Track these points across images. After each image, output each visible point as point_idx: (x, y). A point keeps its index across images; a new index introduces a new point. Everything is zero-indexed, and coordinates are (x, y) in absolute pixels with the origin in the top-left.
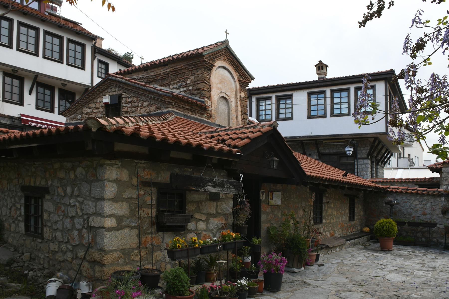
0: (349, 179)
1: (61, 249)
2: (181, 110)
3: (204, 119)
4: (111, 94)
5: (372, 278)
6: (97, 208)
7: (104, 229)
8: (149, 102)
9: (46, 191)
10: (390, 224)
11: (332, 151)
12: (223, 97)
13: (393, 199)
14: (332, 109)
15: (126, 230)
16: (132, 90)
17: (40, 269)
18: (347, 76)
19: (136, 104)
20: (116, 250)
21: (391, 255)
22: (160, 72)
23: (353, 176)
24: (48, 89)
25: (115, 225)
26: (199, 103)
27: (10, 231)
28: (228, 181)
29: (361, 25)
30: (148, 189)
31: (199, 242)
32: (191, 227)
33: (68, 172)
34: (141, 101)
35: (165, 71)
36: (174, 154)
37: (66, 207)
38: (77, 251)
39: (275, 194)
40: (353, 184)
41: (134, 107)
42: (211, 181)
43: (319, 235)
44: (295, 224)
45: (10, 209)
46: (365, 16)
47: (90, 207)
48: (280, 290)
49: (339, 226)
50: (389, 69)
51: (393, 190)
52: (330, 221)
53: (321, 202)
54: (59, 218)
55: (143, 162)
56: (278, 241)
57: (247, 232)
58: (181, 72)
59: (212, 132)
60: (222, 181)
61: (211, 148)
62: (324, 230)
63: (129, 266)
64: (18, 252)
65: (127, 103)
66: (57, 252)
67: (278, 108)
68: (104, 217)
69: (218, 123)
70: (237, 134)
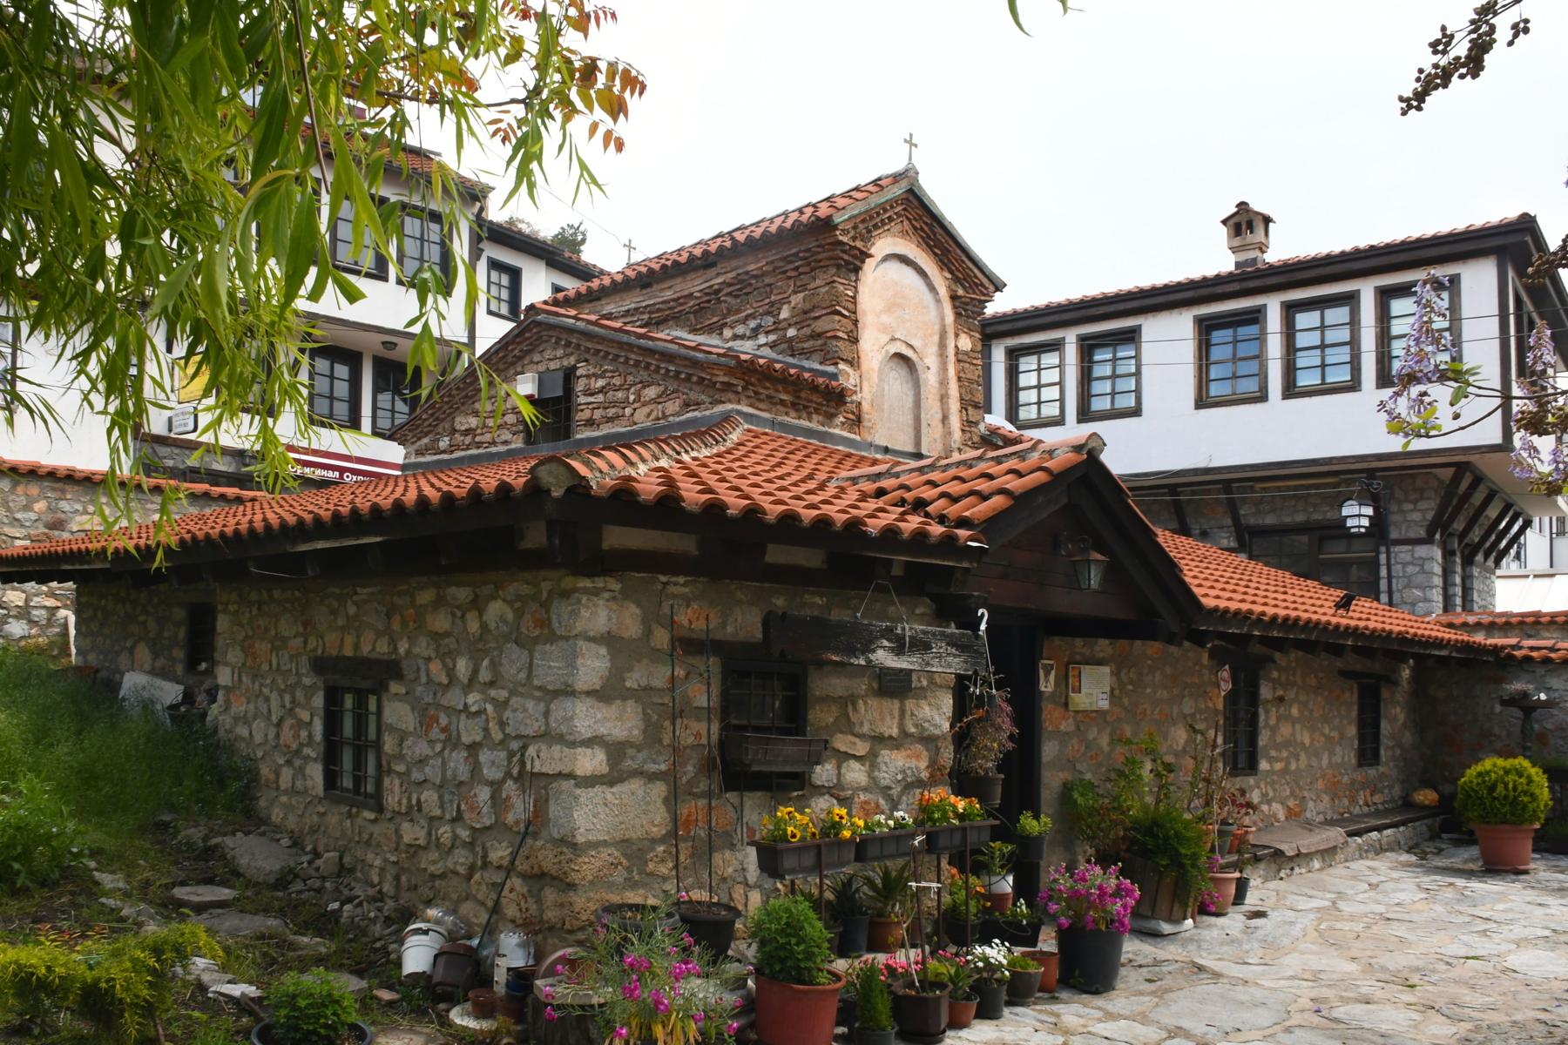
0: (1360, 619)
1: (438, 839)
2: (762, 406)
3: (837, 431)
4: (542, 368)
5: (1448, 963)
6: (552, 719)
7: (573, 782)
8: (662, 388)
9: (390, 670)
10: (1521, 776)
11: (1288, 520)
12: (899, 356)
13: (1531, 687)
14: (1290, 370)
15: (635, 785)
16: (608, 353)
17: (375, 900)
18: (1348, 247)
19: (620, 394)
20: (605, 843)
21: (1524, 888)
22: (692, 290)
23: (1375, 604)
24: (343, 362)
25: (605, 769)
26: (821, 380)
27: (278, 788)
28: (943, 634)
29: (1410, 107)
30: (698, 662)
31: (852, 824)
32: (824, 778)
33: (459, 614)
34: (635, 385)
35: (707, 285)
36: (775, 554)
37: (454, 719)
38: (488, 845)
39: (1087, 671)
40: (1374, 635)
41: (613, 404)
42: (888, 633)
43: (1247, 814)
44: (1158, 775)
45: (279, 725)
46: (1423, 76)
47: (526, 715)
48: (1114, 989)
49: (1320, 781)
50: (1512, 213)
51: (1534, 654)
52: (1288, 763)
53: (1254, 700)
54: (433, 748)
55: (681, 580)
56: (1101, 830)
57: (999, 796)
58: (760, 284)
59: (879, 476)
60: (924, 632)
61: (890, 532)
62: (1264, 795)
63: (641, 891)
64: (303, 849)
65: (592, 395)
66: (425, 848)
67: (1086, 378)
68: (573, 744)
69: (883, 443)
70: (963, 480)
